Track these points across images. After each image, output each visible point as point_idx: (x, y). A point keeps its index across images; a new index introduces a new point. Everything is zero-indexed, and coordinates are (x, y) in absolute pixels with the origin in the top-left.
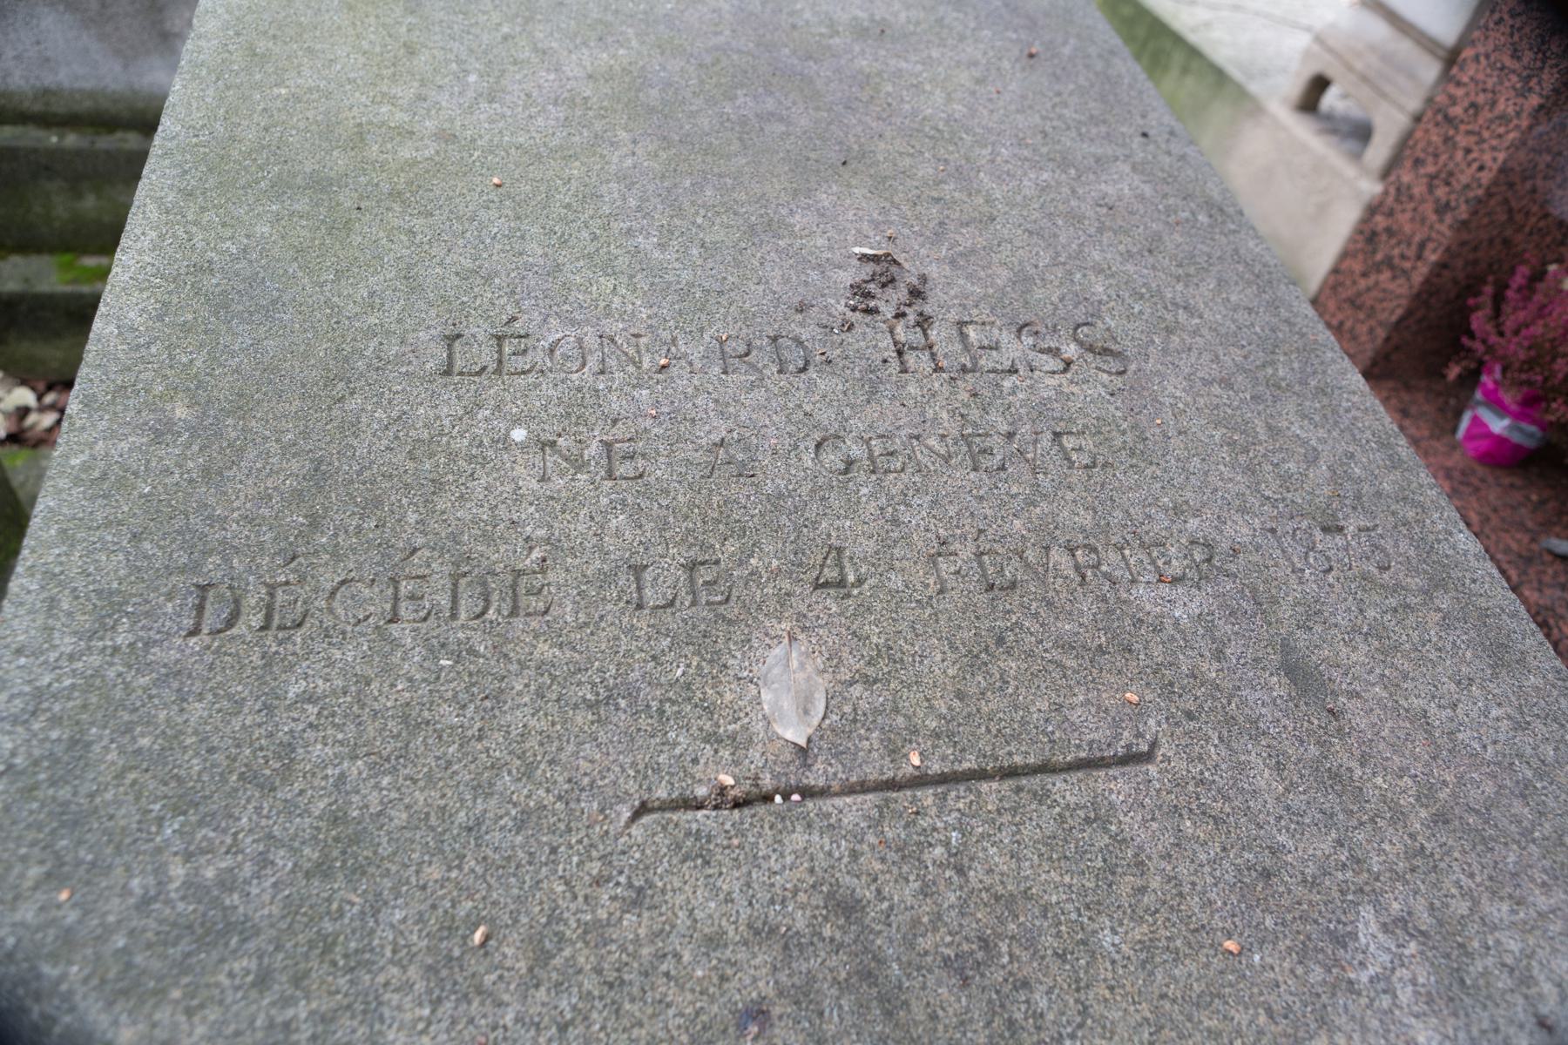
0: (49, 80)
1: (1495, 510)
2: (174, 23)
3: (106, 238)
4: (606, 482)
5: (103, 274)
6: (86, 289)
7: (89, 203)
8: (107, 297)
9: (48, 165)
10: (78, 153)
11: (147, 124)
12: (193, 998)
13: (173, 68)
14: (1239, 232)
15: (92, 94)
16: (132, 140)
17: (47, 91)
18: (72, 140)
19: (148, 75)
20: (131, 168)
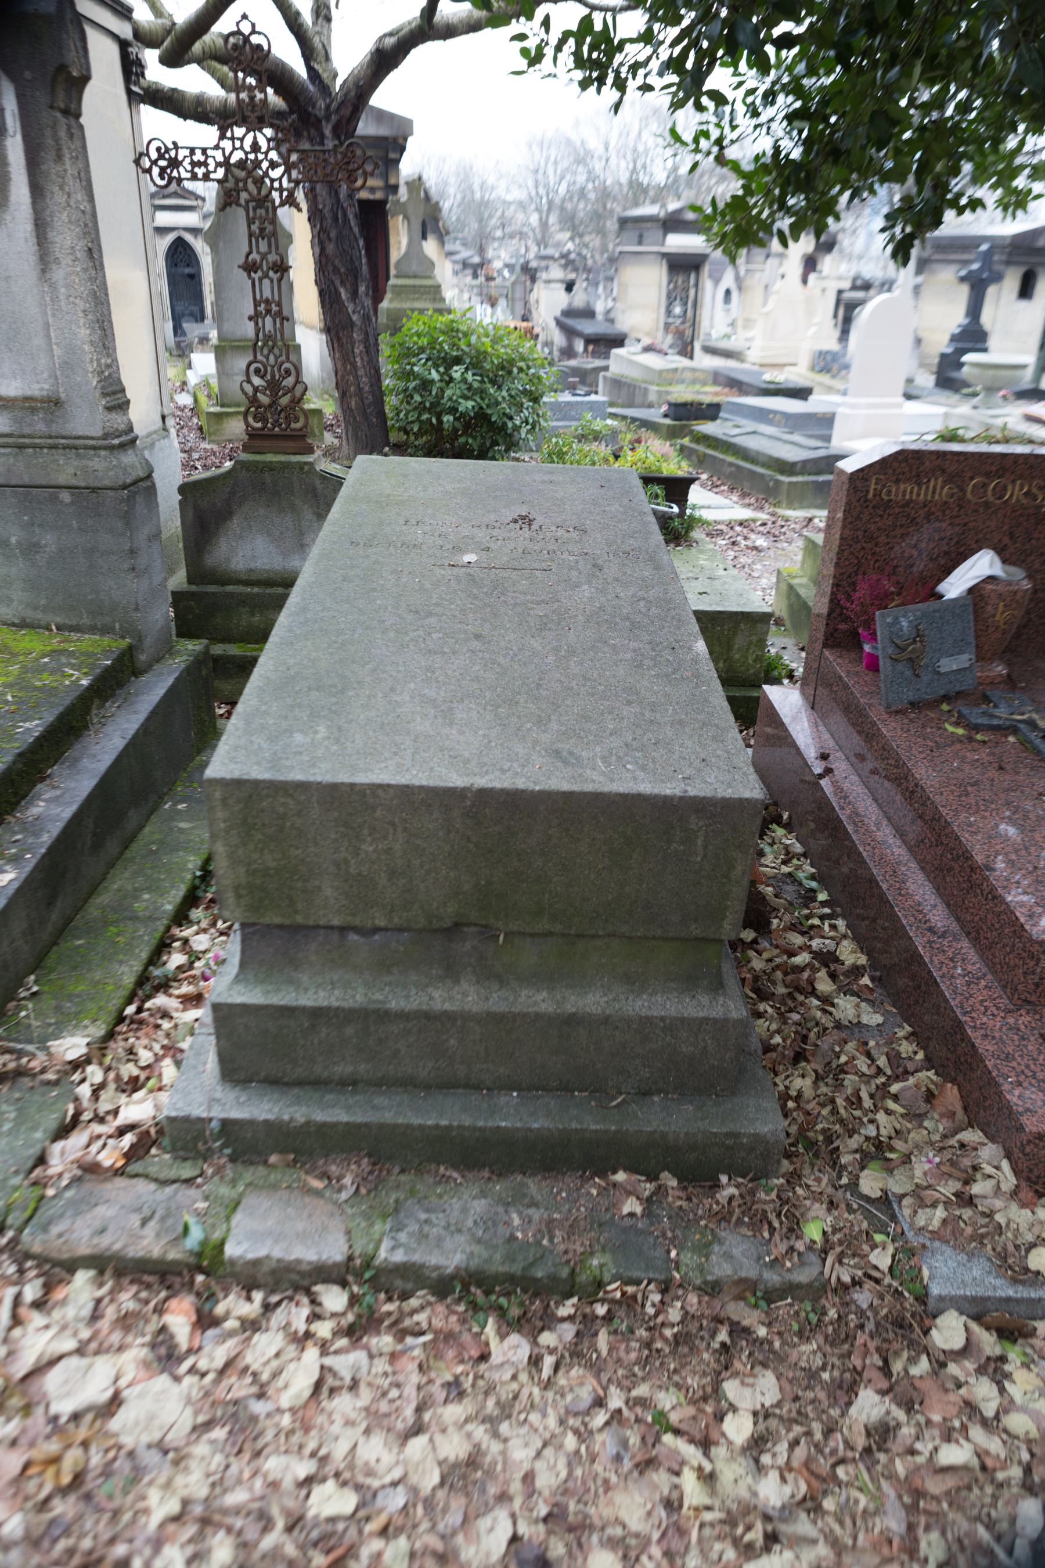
0: (253, 565)
1: (705, 856)
2: (307, 540)
3: (262, 636)
4: (476, 1203)
5: (261, 650)
6: (255, 653)
7: (257, 618)
8: (261, 660)
9: (243, 601)
10: (258, 595)
11: (288, 582)
12: (513, 1261)
13: (304, 559)
14: (525, 392)
15: (267, 571)
16: (280, 590)
17: (251, 570)
18: (256, 590)
19: (293, 563)
20: (279, 603)
